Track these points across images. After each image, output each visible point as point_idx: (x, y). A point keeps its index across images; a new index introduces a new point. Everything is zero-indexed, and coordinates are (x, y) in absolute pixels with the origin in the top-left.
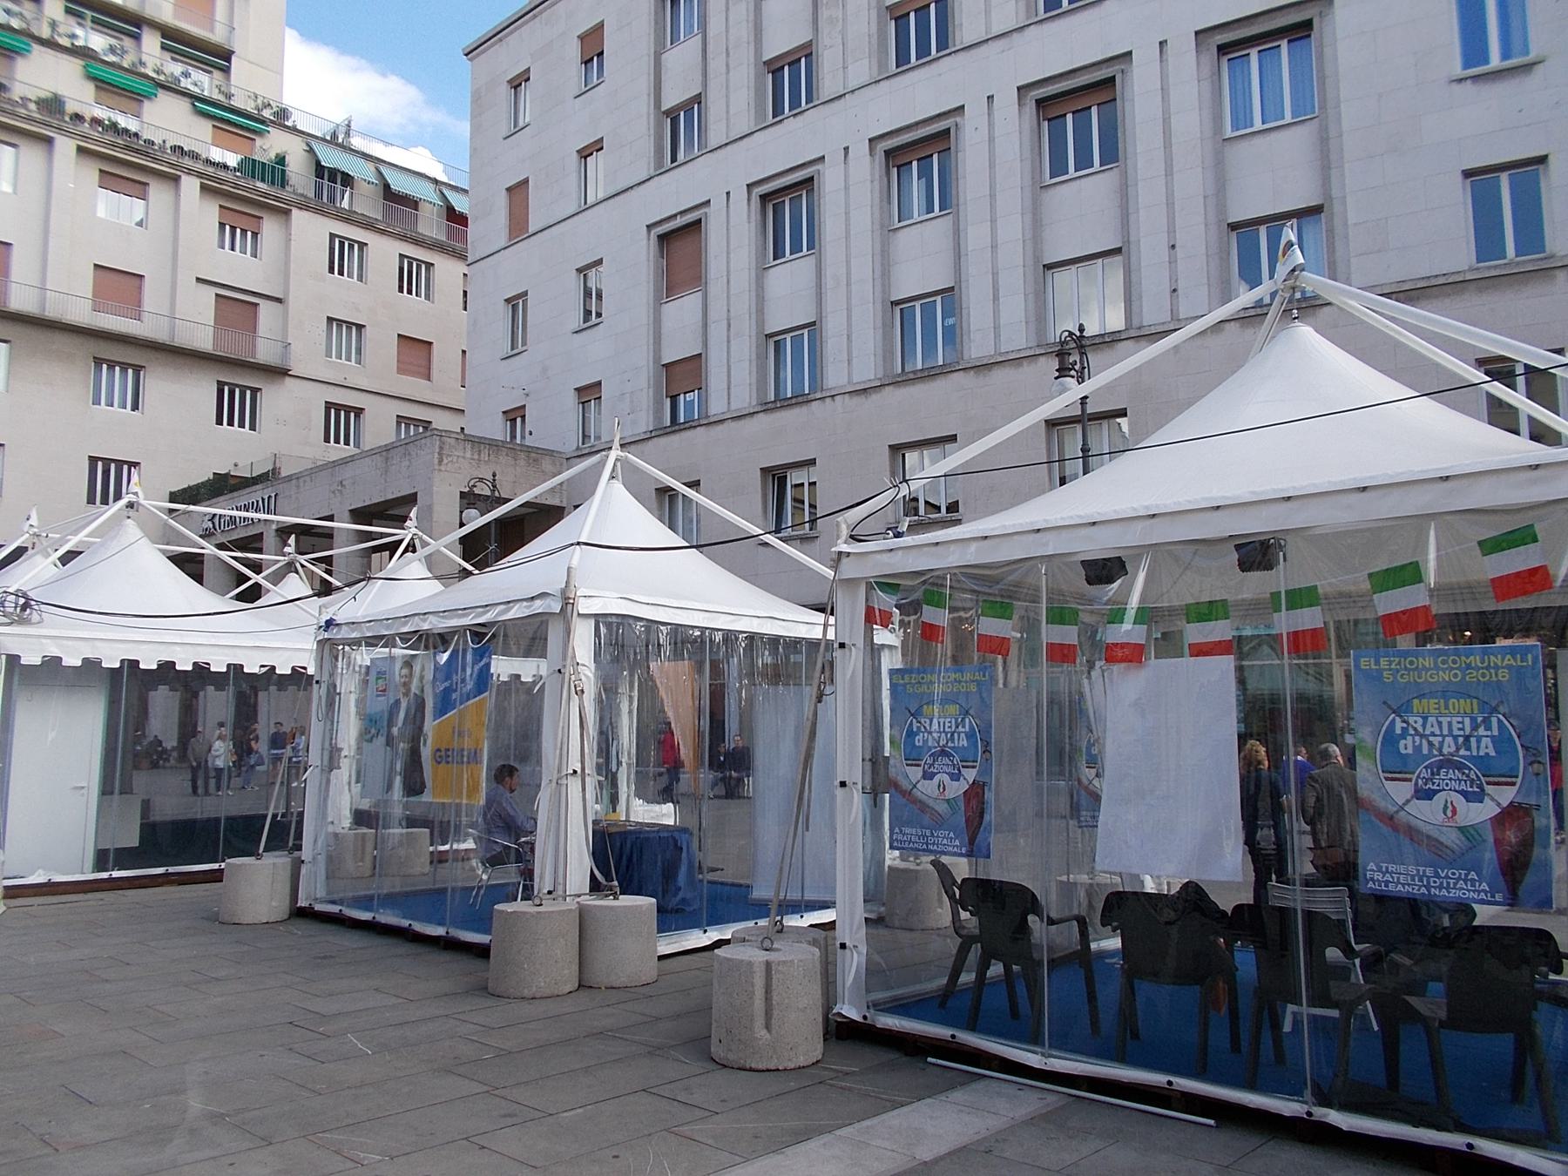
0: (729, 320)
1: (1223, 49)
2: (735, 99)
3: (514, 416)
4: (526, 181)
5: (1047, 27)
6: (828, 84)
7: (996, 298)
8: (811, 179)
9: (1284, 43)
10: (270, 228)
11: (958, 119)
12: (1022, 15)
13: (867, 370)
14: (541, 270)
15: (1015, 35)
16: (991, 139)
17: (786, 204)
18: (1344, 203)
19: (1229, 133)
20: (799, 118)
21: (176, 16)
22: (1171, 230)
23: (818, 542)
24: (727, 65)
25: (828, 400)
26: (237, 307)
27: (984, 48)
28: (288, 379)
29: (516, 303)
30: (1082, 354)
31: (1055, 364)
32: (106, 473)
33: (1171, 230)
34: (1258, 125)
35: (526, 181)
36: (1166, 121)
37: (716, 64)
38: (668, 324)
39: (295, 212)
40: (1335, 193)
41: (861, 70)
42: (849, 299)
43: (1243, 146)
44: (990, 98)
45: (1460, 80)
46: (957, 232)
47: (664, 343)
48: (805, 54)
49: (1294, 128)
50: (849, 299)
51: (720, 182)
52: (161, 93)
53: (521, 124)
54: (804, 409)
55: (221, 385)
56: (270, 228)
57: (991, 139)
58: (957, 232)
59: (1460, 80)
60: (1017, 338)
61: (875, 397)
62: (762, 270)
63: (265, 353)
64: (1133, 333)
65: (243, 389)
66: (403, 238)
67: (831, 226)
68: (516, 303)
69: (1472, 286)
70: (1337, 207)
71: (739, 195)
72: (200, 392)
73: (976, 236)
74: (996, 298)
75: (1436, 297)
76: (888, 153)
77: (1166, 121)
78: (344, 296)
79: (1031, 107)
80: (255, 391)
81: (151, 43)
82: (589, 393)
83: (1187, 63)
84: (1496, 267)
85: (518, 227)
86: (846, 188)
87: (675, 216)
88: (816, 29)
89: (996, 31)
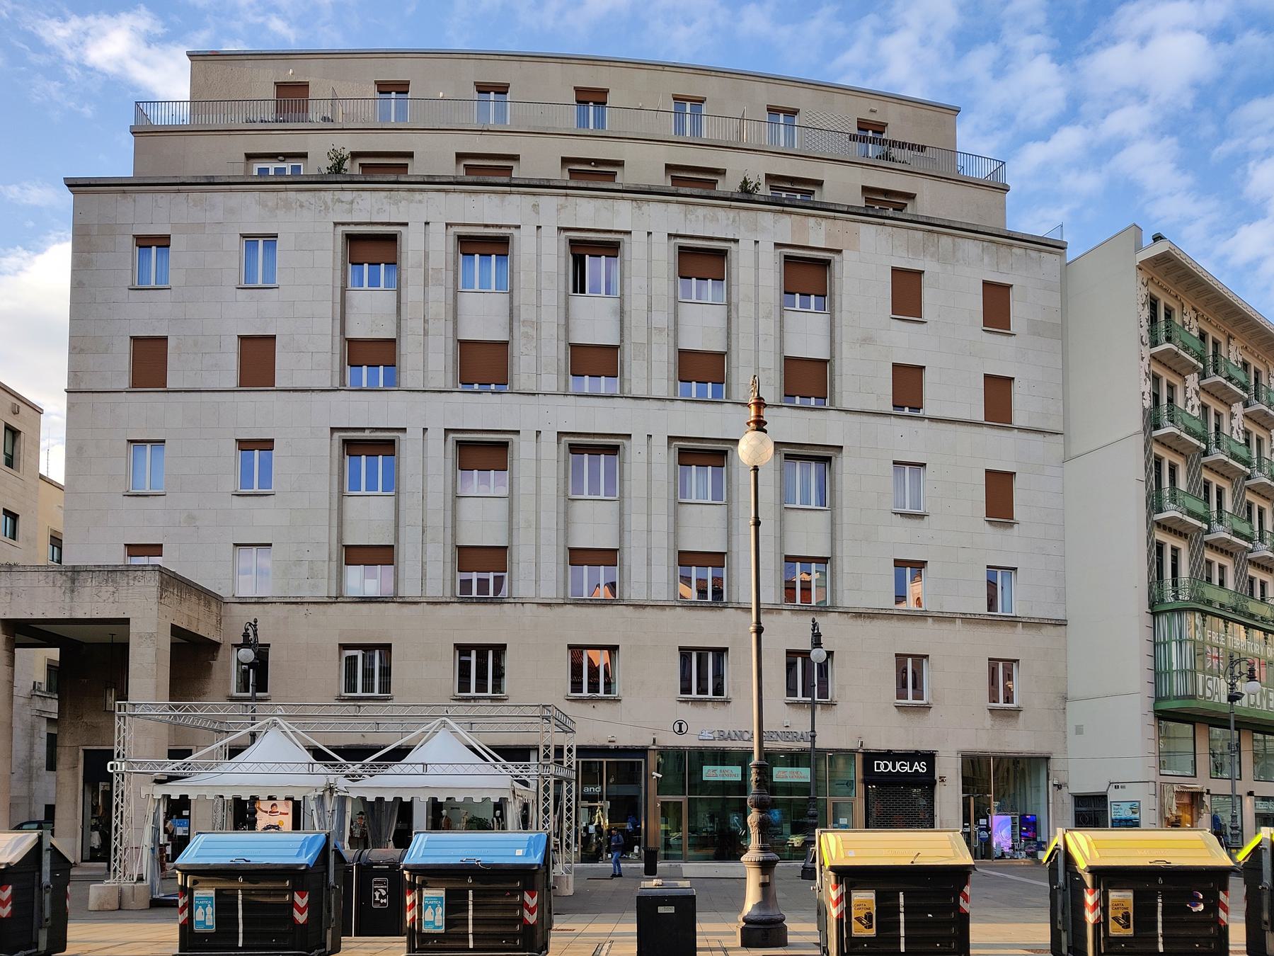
1: (347, 443)
27: (646, 402)
40: (626, 545)
54: (498, 607)
70: (838, 562)
74: (649, 564)
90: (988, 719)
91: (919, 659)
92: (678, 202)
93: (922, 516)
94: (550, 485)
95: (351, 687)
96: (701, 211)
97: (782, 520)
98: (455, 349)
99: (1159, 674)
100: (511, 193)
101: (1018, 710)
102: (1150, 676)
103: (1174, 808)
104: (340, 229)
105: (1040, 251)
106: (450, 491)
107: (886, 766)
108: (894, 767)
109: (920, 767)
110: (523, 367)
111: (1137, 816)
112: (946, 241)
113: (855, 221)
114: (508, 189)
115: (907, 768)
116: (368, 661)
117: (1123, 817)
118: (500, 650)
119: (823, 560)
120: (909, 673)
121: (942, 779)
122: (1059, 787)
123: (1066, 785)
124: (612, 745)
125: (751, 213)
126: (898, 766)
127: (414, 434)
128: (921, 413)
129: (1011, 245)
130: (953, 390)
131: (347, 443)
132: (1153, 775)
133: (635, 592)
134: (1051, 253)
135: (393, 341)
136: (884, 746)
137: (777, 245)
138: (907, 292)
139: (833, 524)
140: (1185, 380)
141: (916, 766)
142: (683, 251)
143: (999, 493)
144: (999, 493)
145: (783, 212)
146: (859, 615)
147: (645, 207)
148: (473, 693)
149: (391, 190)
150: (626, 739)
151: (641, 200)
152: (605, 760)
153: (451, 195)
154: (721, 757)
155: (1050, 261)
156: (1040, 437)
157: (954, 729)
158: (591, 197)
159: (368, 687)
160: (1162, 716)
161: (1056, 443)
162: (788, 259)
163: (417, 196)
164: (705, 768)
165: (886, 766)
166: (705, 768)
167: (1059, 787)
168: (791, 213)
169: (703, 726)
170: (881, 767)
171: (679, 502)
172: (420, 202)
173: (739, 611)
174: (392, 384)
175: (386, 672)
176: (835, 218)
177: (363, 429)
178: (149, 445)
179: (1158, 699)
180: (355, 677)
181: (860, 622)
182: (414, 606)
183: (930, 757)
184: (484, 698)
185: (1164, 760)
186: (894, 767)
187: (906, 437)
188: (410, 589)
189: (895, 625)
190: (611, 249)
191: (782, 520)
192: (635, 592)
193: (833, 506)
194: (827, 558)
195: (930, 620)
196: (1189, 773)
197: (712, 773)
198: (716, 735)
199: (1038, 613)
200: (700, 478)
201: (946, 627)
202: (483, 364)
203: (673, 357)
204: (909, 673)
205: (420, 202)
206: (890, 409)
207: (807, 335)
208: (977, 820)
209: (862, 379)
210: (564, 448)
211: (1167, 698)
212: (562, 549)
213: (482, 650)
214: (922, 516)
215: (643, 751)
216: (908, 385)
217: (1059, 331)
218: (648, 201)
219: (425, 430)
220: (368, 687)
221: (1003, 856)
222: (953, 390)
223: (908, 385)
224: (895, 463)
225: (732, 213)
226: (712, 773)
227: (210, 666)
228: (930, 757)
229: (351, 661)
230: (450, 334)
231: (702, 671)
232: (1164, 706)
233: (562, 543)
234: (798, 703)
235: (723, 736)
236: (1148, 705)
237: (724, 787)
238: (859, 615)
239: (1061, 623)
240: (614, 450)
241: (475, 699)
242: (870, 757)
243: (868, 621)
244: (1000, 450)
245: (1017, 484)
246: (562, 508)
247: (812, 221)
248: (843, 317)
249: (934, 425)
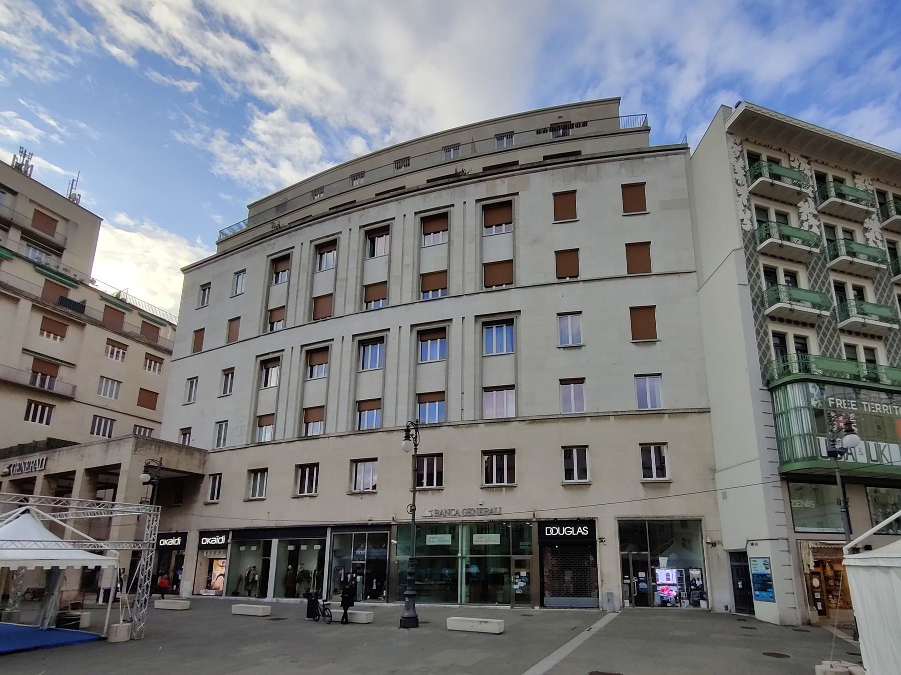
1: (484, 324)
2: (298, 311)
3: (186, 432)
4: (203, 329)
10: (72, 331)
12: (357, 308)
13: (343, 429)
14: (207, 368)
16: (399, 343)
21: (32, 226)
22: (462, 387)
23: (443, 492)
26: (46, 366)
28: (72, 402)
29: (193, 381)
31: (404, 434)
32: (100, 424)
33: (462, 387)
34: (429, 361)
35: (203, 329)
37: (293, 295)
39: (88, 326)
43: (489, 359)
48: (443, 274)
52: (16, 260)
55: (30, 402)
56: (72, 331)
57: (399, 343)
60: (469, 416)
61: (346, 439)
63: (58, 388)
65: (44, 406)
66: (150, 345)
68: (193, 381)
71: (297, 349)
72: (19, 403)
73: (391, 379)
76: (359, 341)
78: (113, 366)
80: (51, 407)
81: (14, 235)
82: (222, 424)
85: (197, 347)
87: (268, 354)
88: (389, 277)
90: (641, 492)
94: (471, 347)
95: (302, 491)
97: (481, 364)
98: (416, 280)
99: (781, 442)
101: (669, 482)
102: (774, 444)
103: (812, 564)
104: (363, 230)
105: (667, 155)
106: (478, 352)
107: (555, 531)
108: (561, 532)
109: (583, 531)
110: (455, 284)
111: (768, 571)
112: (592, 168)
113: (526, 173)
115: (572, 532)
116: (430, 466)
117: (760, 572)
120: (575, 461)
121: (601, 540)
122: (714, 545)
123: (720, 543)
124: (370, 523)
126: (564, 530)
127: (457, 322)
129: (643, 157)
130: (602, 256)
132: (784, 532)
133: (454, 416)
134: (676, 154)
135: (511, 261)
137: (477, 201)
138: (565, 206)
139: (516, 362)
140: (798, 208)
141: (579, 530)
142: (485, 208)
143: (643, 324)
144: (643, 324)
145: (480, 181)
146: (533, 421)
147: (403, 202)
154: (436, 528)
155: (677, 160)
156: (676, 277)
157: (613, 498)
159: (500, 480)
160: (788, 478)
161: (692, 279)
162: (484, 207)
164: (428, 536)
165: (555, 531)
166: (428, 536)
167: (714, 545)
168: (485, 180)
169: (429, 506)
170: (551, 531)
175: (511, 468)
176: (513, 175)
179: (783, 463)
183: (590, 523)
185: (796, 517)
186: (561, 532)
187: (568, 296)
188: (330, 430)
190: (384, 230)
191: (481, 364)
192: (454, 416)
193: (516, 350)
195: (612, 418)
196: (842, 530)
197: (433, 540)
198: (433, 513)
199: (682, 405)
201: (601, 423)
204: (575, 461)
207: (498, 247)
208: (636, 575)
209: (534, 265)
210: (479, 325)
211: (789, 462)
213: (500, 453)
215: (388, 526)
216: (567, 264)
217: (687, 202)
220: (500, 480)
221: (664, 603)
222: (602, 256)
223: (567, 264)
226: (433, 540)
228: (590, 523)
230: (478, 260)
232: (789, 468)
233: (478, 384)
234: (493, 487)
235: (438, 513)
236: (775, 469)
238: (533, 421)
239: (706, 411)
240: (381, 340)
241: (579, 484)
243: (540, 425)
244: (642, 291)
245: (657, 312)
246: (478, 363)
248: (520, 232)
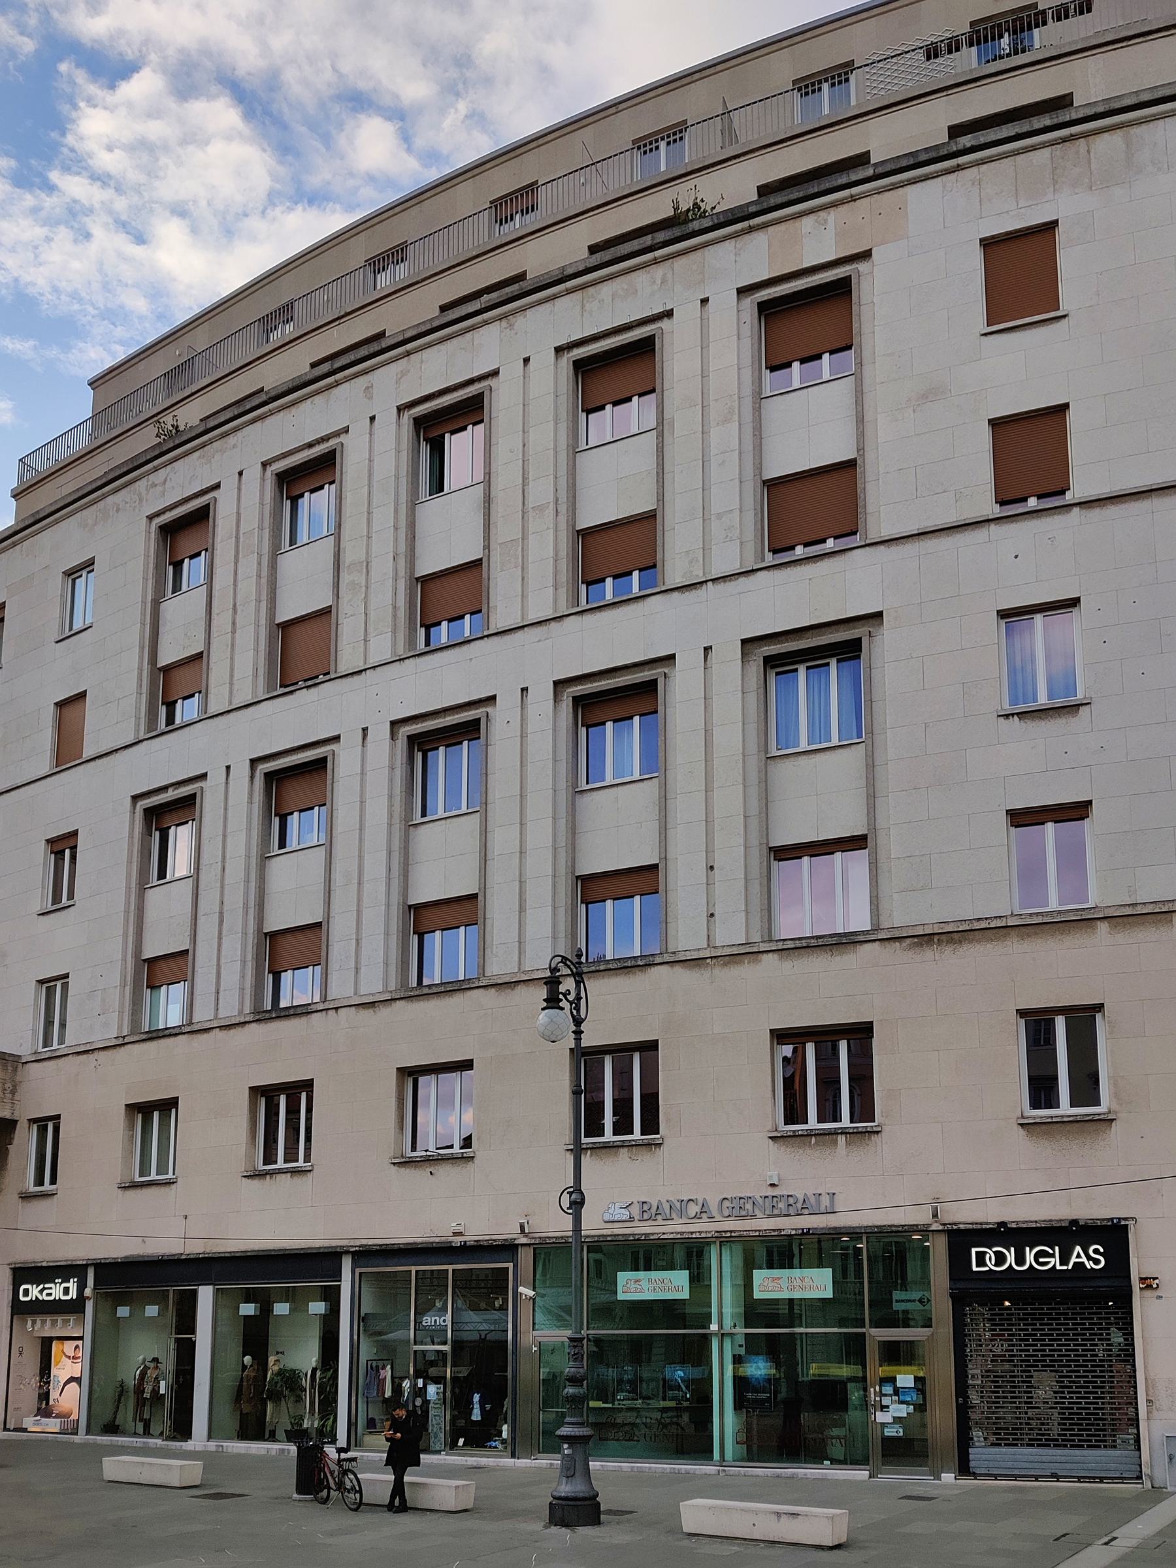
0: (221, 913)
1: (770, 662)
2: (238, 665)
5: (588, 618)
6: (348, 657)
7: (522, 909)
8: (325, 759)
9: (833, 663)
11: (489, 709)
15: (553, 624)
17: (293, 782)
18: (888, 835)
19: (774, 752)
20: (313, 690)
22: (709, 851)
24: (234, 623)
25: (330, 1012)
27: (520, 634)
30: (578, 983)
31: (543, 992)
36: (708, 732)
37: (222, 621)
38: (152, 914)
40: (881, 823)
41: (381, 648)
42: (359, 900)
43: (788, 764)
44: (524, 690)
45: (1007, 716)
46: (871, 766)
47: (147, 935)
49: (840, 751)
50: (359, 900)
51: (220, 748)
53: (77, 626)
54: (304, 1019)
57: (523, 736)
58: (871, 766)
59: (1007, 716)
61: (384, 1012)
62: (410, 826)
64: (667, 958)
67: (503, 785)
69: (1013, 932)
70: (882, 840)
71: (241, 771)
74: (522, 909)
75: (979, 941)
77: (708, 732)
79: (566, 705)
83: (733, 676)
84: (1037, 914)
86: (363, 773)
89: (532, 617)
91: (1083, 1019)
92: (569, 292)
93: (1074, 708)
96: (606, 290)
100: (337, 384)
108: (1020, 1260)
109: (1089, 1257)
114: (331, 379)
118: (860, 1034)
119: (856, 842)
124: (457, 1241)
125: (693, 256)
128: (1069, 497)
131: (770, 662)
133: (687, 936)
136: (990, 1214)
145: (751, 229)
148: (813, 1123)
149: (203, 445)
150: (482, 1226)
151: (514, 313)
152: (450, 1268)
153: (270, 421)
154: (646, 1254)
158: (441, 341)
163: (232, 440)
168: (765, 226)
169: (622, 1193)
170: (988, 1260)
171: (771, 752)
172: (234, 446)
173: (678, 969)
174: (654, 588)
177: (164, 789)
178: (1038, 618)
180: (276, 1141)
181: (929, 954)
182: (205, 1036)
184: (835, 1133)
186: (1020, 1260)
189: (1015, 950)
192: (687, 936)
194: (863, 838)
197: (636, 1286)
198: (635, 1211)
200: (815, 694)
202: (614, 556)
203: (752, 494)
205: (234, 446)
206: (997, 511)
210: (756, 667)
212: (395, 911)
213: (825, 1036)
214: (1074, 708)
215: (508, 1249)
218: (523, 309)
219: (707, 649)
224: (1003, 614)
225: (658, 272)
226: (636, 1286)
227: (7, 1150)
229: (794, 1066)
231: (616, 1095)
233: (395, 898)
234: (810, 1134)
235: (649, 1212)
237: (667, 1311)
240: (471, 730)
242: (962, 1239)
243: (948, 950)
246: (753, 777)
247: (808, 222)
249: (1096, 513)
